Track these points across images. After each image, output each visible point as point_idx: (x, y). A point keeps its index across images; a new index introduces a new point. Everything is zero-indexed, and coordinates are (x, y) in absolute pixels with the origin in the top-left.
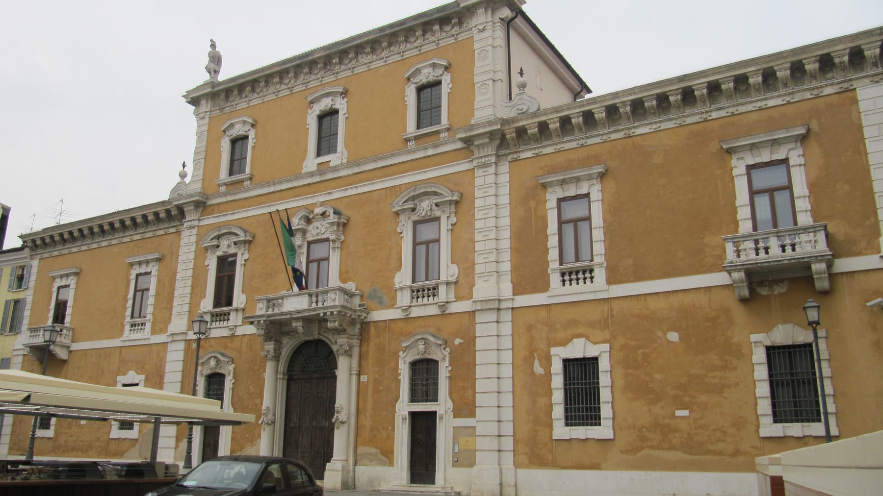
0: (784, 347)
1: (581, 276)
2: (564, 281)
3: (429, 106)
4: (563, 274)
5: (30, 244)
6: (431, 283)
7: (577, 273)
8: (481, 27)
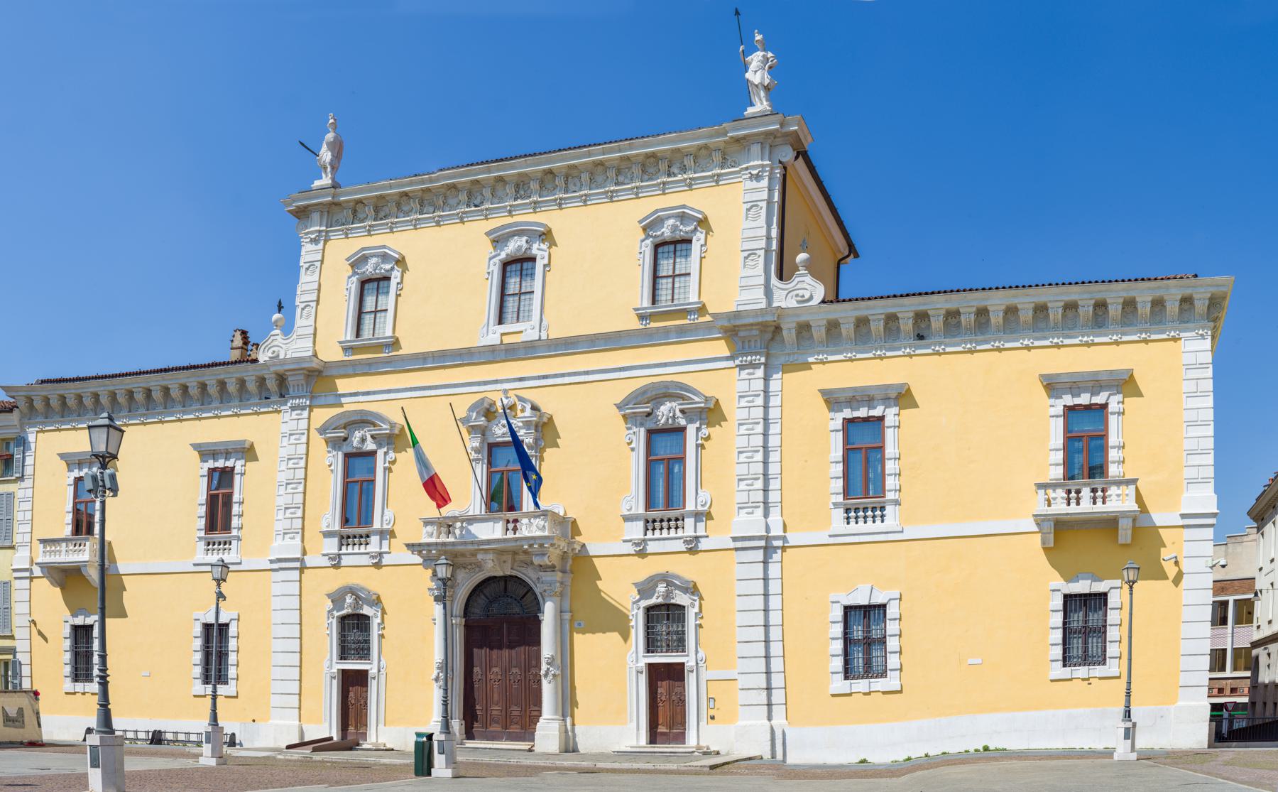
0: (1080, 595)
1: (870, 513)
2: (848, 518)
3: (670, 273)
4: (847, 511)
5: (22, 404)
6: (672, 514)
7: (865, 510)
8: (754, 172)
